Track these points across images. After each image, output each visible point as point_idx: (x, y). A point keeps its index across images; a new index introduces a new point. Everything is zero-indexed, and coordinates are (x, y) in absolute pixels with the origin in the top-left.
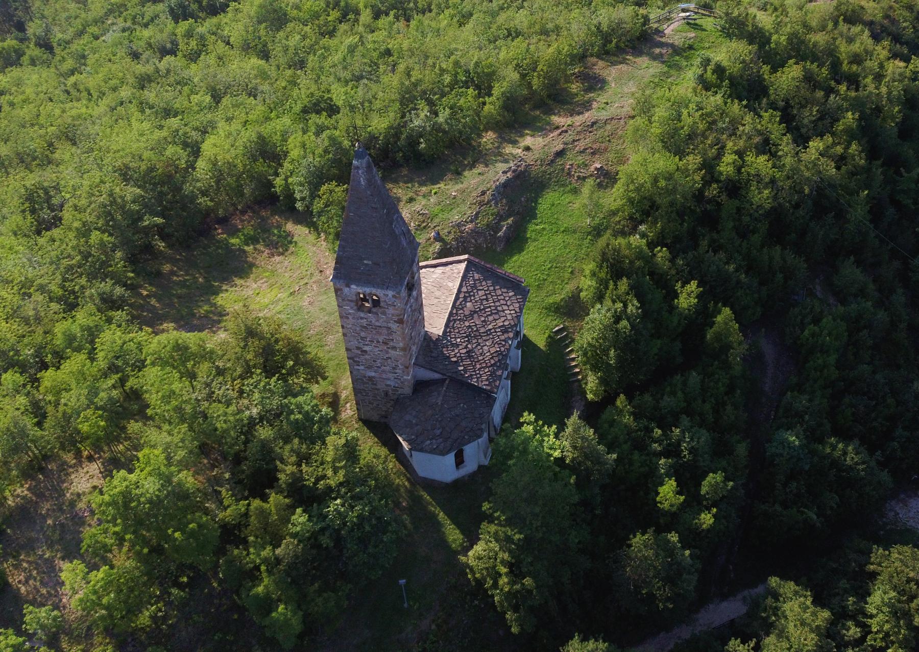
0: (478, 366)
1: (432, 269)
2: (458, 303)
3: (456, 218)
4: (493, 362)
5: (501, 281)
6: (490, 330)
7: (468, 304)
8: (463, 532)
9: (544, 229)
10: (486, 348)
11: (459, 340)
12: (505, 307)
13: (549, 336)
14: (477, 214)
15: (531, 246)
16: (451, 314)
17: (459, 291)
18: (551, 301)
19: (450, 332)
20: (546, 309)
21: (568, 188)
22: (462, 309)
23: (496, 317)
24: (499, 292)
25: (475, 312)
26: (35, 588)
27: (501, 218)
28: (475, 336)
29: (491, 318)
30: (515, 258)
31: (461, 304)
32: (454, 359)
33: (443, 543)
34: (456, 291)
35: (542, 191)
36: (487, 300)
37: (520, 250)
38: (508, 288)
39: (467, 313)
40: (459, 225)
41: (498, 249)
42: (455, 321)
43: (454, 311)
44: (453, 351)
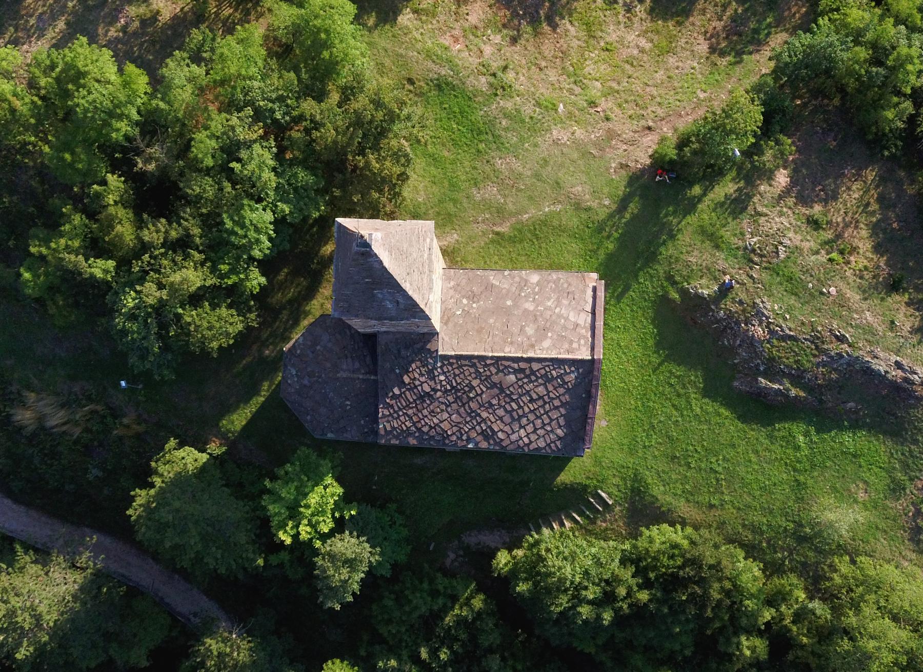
0: (410, 412)
1: (589, 308)
2: (507, 363)
3: (770, 306)
4: (425, 429)
5: (579, 413)
6: (479, 415)
7: (512, 378)
8: (245, 428)
9: (797, 448)
10: (445, 415)
11: (442, 378)
12: (530, 428)
13: (585, 487)
14: (793, 338)
15: (757, 434)
16: (482, 358)
17: (530, 360)
18: (649, 481)
19: (451, 364)
20: (635, 475)
21: (899, 475)
22: (499, 371)
23: (507, 419)
24: (554, 415)
25: (502, 390)
26: (35, 10)
27: (797, 378)
28: (457, 398)
29: (501, 412)
30: (724, 412)
31: (506, 367)
32: (406, 379)
33: (228, 409)
34: (531, 354)
35: (885, 433)
36: (532, 400)
37: (744, 417)
38: (568, 424)
39: (495, 379)
40: (759, 314)
41: (736, 384)
42: (474, 365)
43: (488, 362)
44: (421, 375)
